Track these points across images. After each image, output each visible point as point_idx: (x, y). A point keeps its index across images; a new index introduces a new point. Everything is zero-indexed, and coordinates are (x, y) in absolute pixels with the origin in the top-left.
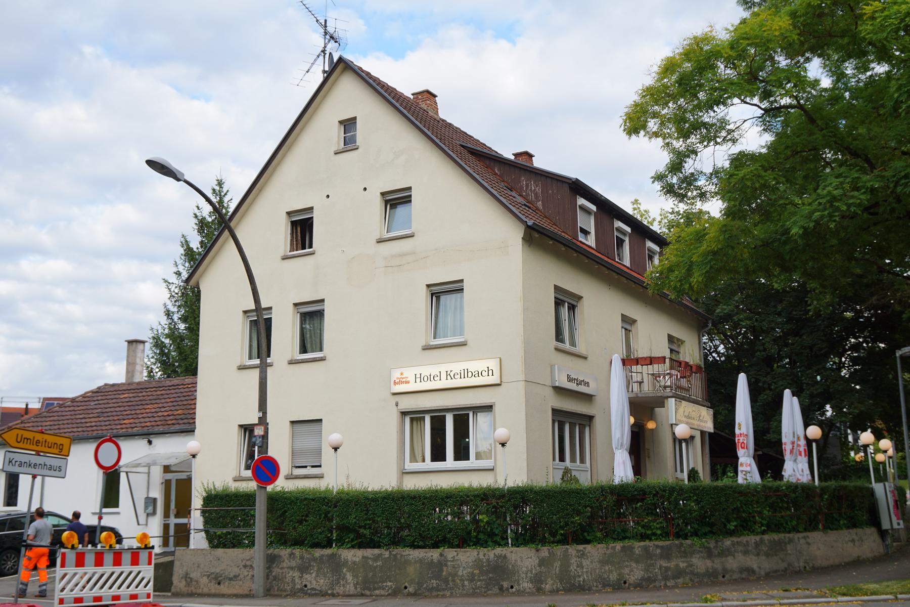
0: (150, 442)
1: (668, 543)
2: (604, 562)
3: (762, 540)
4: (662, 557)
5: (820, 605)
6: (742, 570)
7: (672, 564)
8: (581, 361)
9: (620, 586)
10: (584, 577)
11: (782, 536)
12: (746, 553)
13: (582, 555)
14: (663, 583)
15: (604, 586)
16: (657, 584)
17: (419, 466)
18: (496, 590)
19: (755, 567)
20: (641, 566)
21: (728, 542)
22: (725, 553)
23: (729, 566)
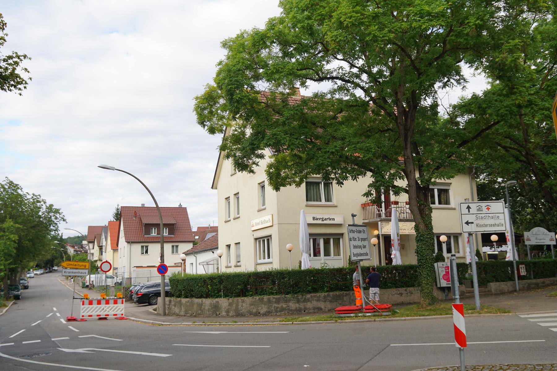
0: (213, 252)
1: (279, 296)
2: (251, 304)
3: (328, 295)
4: (275, 302)
5: (164, 326)
6: (314, 309)
7: (280, 306)
8: (335, 208)
9: (257, 314)
10: (243, 311)
11: (342, 292)
12: (318, 301)
13: (243, 302)
14: (275, 314)
15: (250, 314)
16: (272, 314)
17: (262, 261)
18: (215, 315)
19: (323, 307)
20: (266, 306)
21: (308, 296)
22: (306, 301)
23: (308, 307)
